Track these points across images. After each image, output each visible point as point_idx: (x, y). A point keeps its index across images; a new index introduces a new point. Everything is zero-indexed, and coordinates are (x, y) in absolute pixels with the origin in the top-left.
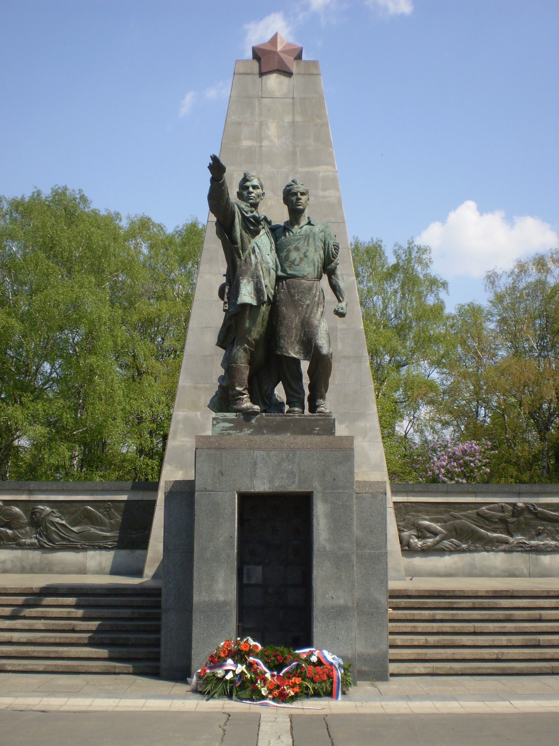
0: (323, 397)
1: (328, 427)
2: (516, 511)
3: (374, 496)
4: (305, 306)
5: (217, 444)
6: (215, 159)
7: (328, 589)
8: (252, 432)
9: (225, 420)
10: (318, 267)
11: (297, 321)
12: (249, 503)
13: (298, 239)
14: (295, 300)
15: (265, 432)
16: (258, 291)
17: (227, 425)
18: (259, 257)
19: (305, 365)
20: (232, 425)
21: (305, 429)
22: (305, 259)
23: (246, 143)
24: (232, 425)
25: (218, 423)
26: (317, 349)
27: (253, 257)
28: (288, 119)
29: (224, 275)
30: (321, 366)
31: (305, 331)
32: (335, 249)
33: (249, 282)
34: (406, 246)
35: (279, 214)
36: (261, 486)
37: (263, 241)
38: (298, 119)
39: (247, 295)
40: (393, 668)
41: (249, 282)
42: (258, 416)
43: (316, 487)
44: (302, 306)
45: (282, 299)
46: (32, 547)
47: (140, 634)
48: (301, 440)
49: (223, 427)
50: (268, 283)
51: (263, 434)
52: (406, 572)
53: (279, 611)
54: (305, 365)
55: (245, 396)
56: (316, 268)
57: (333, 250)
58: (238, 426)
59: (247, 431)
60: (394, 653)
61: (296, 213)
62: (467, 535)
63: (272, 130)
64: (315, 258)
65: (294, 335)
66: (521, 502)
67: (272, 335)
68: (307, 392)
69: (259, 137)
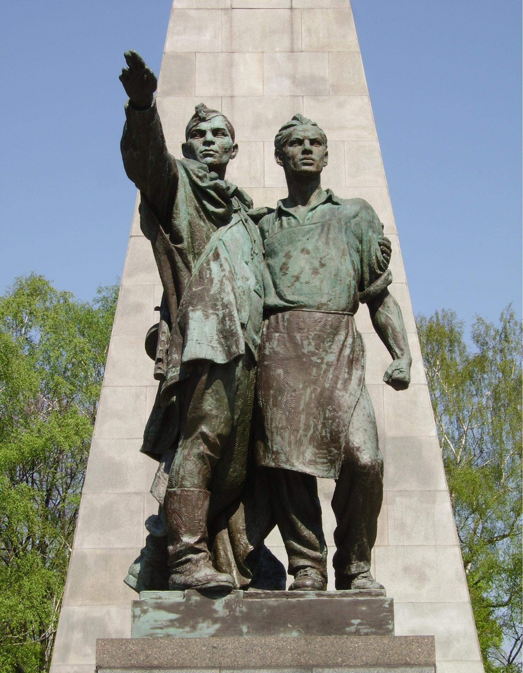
0: (365, 557)
4: (324, 366)
5: (142, 657)
6: (133, 60)
8: (218, 630)
9: (159, 607)
10: (349, 287)
13: (308, 232)
14: (304, 354)
15: (245, 629)
16: (226, 335)
17: (166, 616)
18: (226, 267)
19: (326, 488)
20: (174, 616)
22: (321, 270)
24: (174, 616)
25: (144, 612)
27: (214, 266)
29: (157, 309)
31: (325, 418)
32: (383, 252)
33: (207, 317)
41: (207, 317)
42: (228, 597)
44: (318, 366)
45: (276, 353)
49: (156, 621)
51: (241, 634)
54: (326, 488)
55: (202, 554)
56: (346, 287)
57: (379, 254)
59: (206, 629)
64: (343, 268)
65: (302, 426)
68: (332, 549)
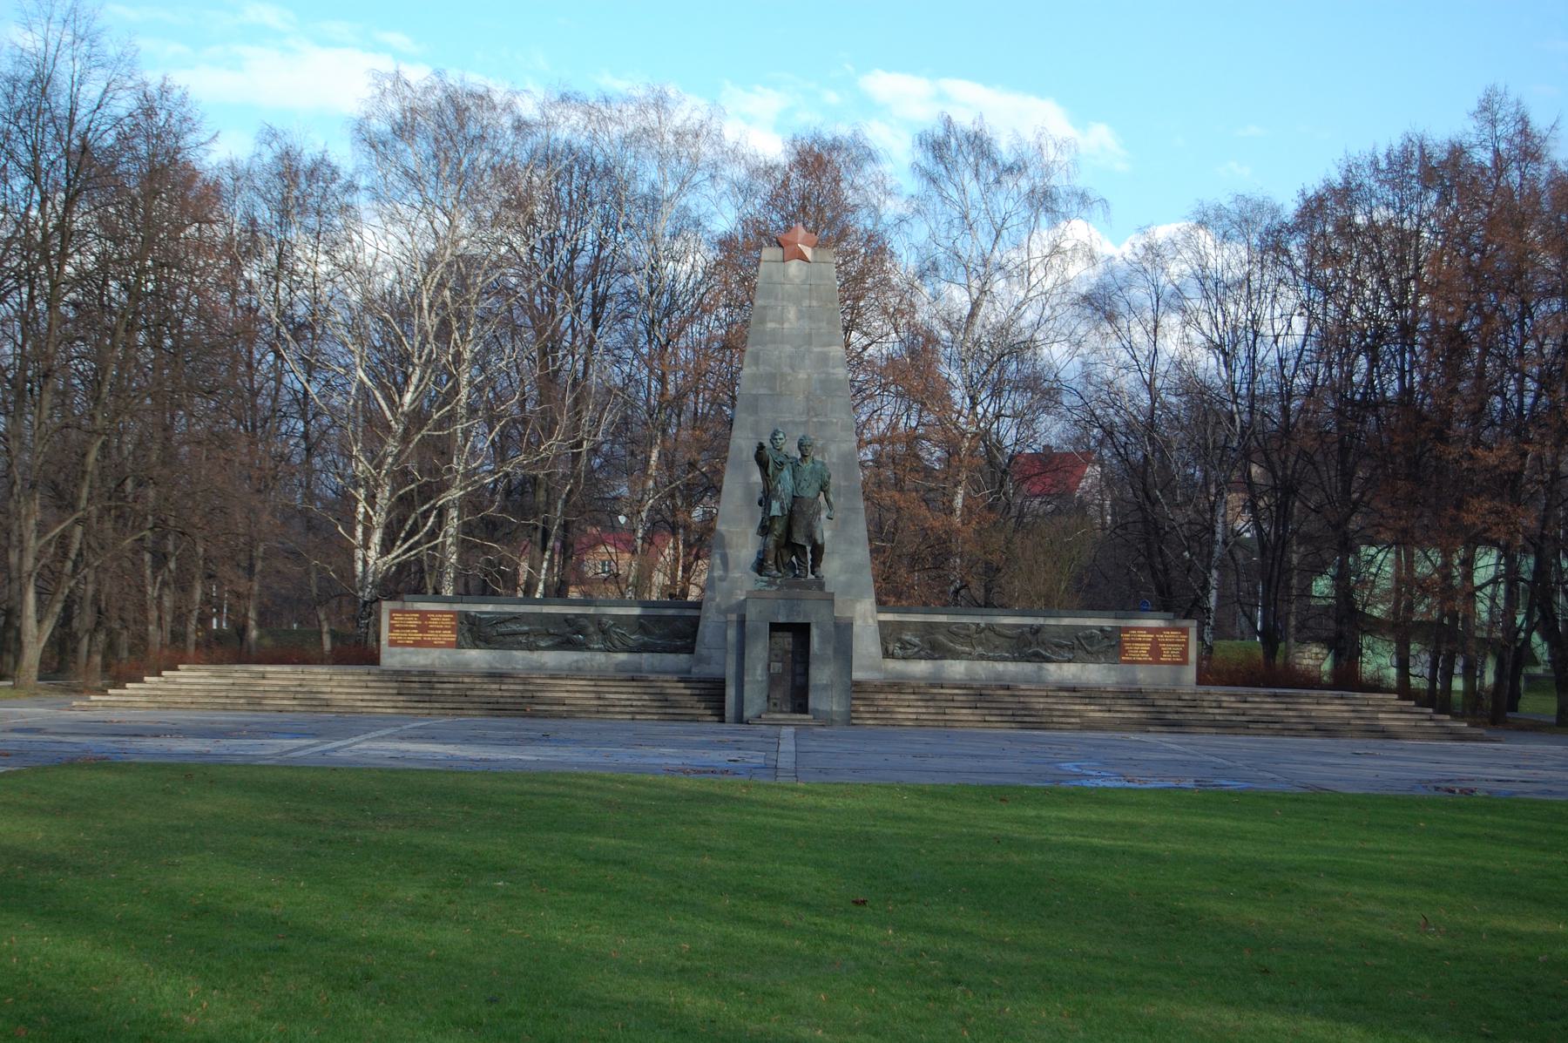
7: (821, 674)
16: (782, 508)
19: (809, 549)
28: (806, 303)
30: (818, 551)
36: (782, 620)
37: (786, 474)
38: (814, 303)
39: (776, 509)
43: (812, 620)
46: (600, 650)
50: (787, 502)
53: (795, 692)
54: (809, 549)
58: (770, 584)
63: (792, 313)
67: (789, 530)
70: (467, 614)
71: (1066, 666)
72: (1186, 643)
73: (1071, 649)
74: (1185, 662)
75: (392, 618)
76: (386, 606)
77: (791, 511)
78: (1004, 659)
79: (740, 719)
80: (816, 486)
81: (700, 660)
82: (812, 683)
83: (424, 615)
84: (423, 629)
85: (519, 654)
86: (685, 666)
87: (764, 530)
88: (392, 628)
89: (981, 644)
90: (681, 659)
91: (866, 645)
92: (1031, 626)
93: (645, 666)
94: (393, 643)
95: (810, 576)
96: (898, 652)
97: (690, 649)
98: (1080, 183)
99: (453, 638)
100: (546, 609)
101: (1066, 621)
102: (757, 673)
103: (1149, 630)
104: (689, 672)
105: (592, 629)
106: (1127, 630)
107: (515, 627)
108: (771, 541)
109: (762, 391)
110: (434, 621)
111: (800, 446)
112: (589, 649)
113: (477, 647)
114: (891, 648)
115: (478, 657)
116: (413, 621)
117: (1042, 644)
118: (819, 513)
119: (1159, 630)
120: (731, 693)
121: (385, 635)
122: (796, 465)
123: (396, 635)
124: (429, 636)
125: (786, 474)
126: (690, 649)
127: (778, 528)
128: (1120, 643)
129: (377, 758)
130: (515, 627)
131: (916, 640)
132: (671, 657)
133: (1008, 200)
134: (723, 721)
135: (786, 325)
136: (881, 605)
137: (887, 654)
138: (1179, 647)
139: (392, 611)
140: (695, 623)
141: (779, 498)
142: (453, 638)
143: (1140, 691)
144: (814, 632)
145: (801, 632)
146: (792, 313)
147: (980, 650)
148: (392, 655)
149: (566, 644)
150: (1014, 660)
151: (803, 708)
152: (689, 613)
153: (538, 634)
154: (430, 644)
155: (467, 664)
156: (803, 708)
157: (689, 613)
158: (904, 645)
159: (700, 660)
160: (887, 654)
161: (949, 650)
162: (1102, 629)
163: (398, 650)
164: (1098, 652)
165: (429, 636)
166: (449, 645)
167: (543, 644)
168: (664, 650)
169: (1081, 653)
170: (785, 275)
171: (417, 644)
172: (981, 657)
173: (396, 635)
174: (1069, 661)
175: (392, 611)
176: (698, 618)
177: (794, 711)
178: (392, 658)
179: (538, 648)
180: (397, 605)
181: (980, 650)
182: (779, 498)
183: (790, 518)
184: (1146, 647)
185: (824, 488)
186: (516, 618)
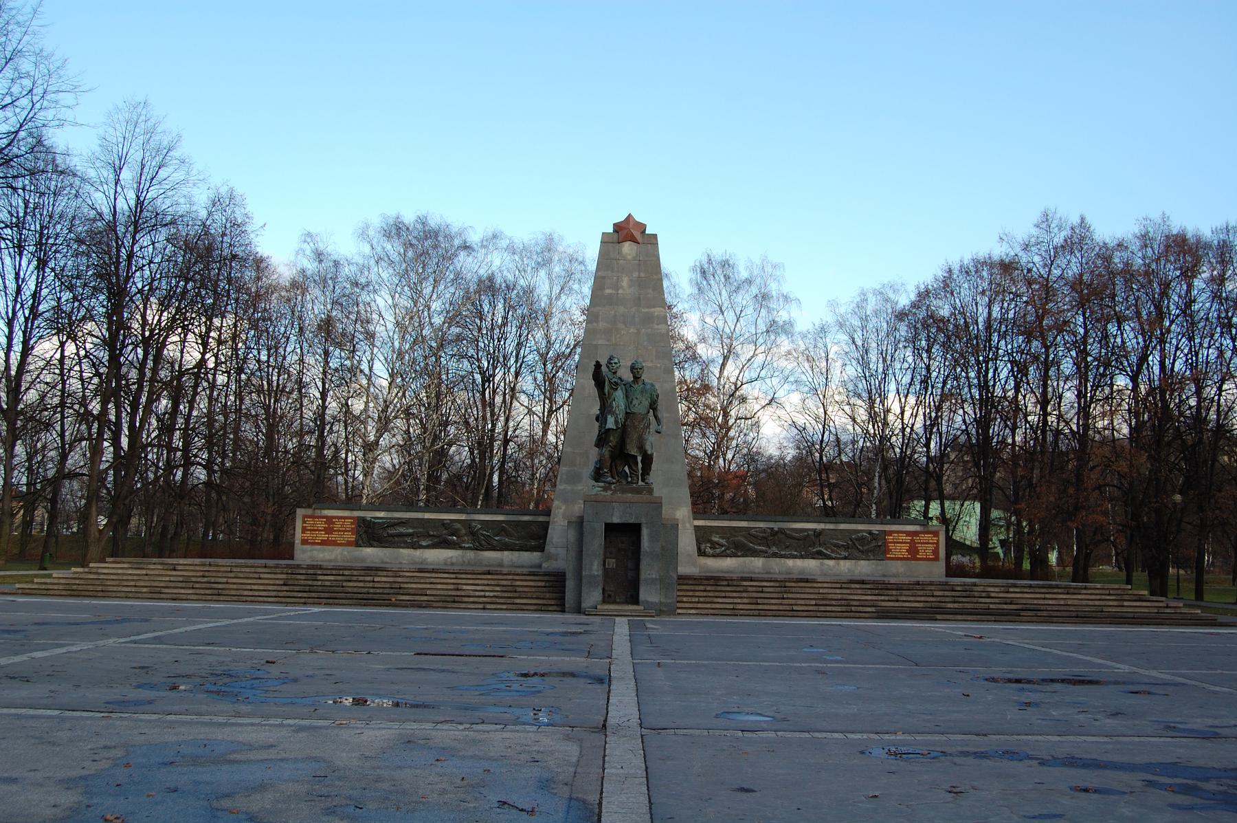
1: (650, 491)
2: (773, 533)
3: (672, 526)
7: (649, 570)
11: (636, 436)
12: (610, 528)
16: (616, 422)
19: (639, 459)
21: (638, 491)
23: (608, 291)
26: (646, 451)
28: (636, 275)
30: (648, 460)
34: (758, 262)
35: (628, 377)
36: (616, 520)
37: (619, 394)
38: (642, 275)
39: (611, 423)
40: (679, 611)
43: (643, 520)
46: (469, 548)
47: (555, 591)
48: (637, 497)
50: (621, 416)
52: (690, 563)
53: (623, 587)
54: (639, 459)
58: (605, 489)
60: (679, 605)
61: (636, 378)
62: (739, 546)
63: (625, 282)
66: (776, 526)
67: (622, 442)
69: (617, 287)
70: (363, 519)
71: (842, 562)
72: (937, 544)
73: (847, 548)
74: (937, 559)
75: (304, 522)
76: (300, 512)
77: (624, 426)
78: (795, 557)
79: (579, 610)
80: (646, 403)
81: (549, 558)
82: (643, 576)
83: (330, 519)
84: (329, 531)
85: (405, 552)
86: (537, 561)
87: (601, 441)
88: (304, 530)
89: (774, 544)
90: (528, 558)
91: (686, 541)
92: (815, 530)
93: (506, 562)
94: (304, 542)
95: (640, 483)
96: (708, 550)
97: (541, 548)
98: (785, 289)
99: (352, 538)
100: (427, 516)
101: (842, 526)
102: (594, 568)
103: (908, 533)
104: (540, 566)
105: (463, 532)
106: (890, 533)
107: (402, 530)
108: (606, 451)
109: (600, 342)
110: (337, 526)
111: (633, 368)
112: (462, 548)
113: (371, 546)
114: (703, 547)
115: (371, 554)
116: (321, 525)
117: (824, 544)
118: (648, 427)
119: (916, 533)
120: (570, 584)
121: (299, 535)
122: (628, 388)
123: (308, 535)
124: (334, 536)
125: (619, 394)
126: (541, 548)
127: (613, 440)
128: (885, 543)
129: (718, 571)
130: (402, 530)
131: (723, 542)
132: (526, 554)
133: (744, 299)
134: (563, 611)
135: (620, 291)
136: (698, 513)
137: (701, 553)
138: (931, 547)
139: (305, 517)
140: (545, 527)
141: (613, 413)
142: (352, 538)
143: (918, 583)
144: (645, 532)
145: (632, 531)
146: (625, 282)
147: (774, 549)
148: (304, 552)
149: (443, 544)
150: (802, 557)
151: (635, 600)
152: (541, 519)
153: (420, 535)
154: (334, 543)
155: (363, 560)
156: (635, 600)
157: (541, 519)
158: (714, 545)
159: (549, 558)
160: (701, 553)
161: (750, 549)
162: (870, 533)
163: (308, 547)
164: (868, 551)
165: (334, 536)
166: (349, 544)
167: (424, 544)
168: (522, 549)
169: (856, 553)
170: (620, 253)
171: (323, 543)
172: (775, 555)
173: (308, 535)
174: (845, 558)
175: (305, 517)
176: (548, 523)
177: (627, 603)
178: (305, 555)
179: (421, 547)
180: (309, 512)
181: (774, 549)
182: (613, 413)
183: (623, 431)
184: (906, 547)
185: (653, 406)
186: (403, 523)
